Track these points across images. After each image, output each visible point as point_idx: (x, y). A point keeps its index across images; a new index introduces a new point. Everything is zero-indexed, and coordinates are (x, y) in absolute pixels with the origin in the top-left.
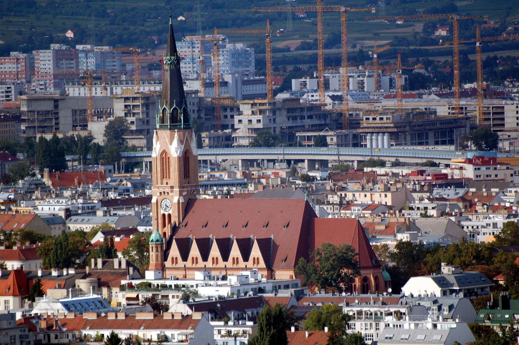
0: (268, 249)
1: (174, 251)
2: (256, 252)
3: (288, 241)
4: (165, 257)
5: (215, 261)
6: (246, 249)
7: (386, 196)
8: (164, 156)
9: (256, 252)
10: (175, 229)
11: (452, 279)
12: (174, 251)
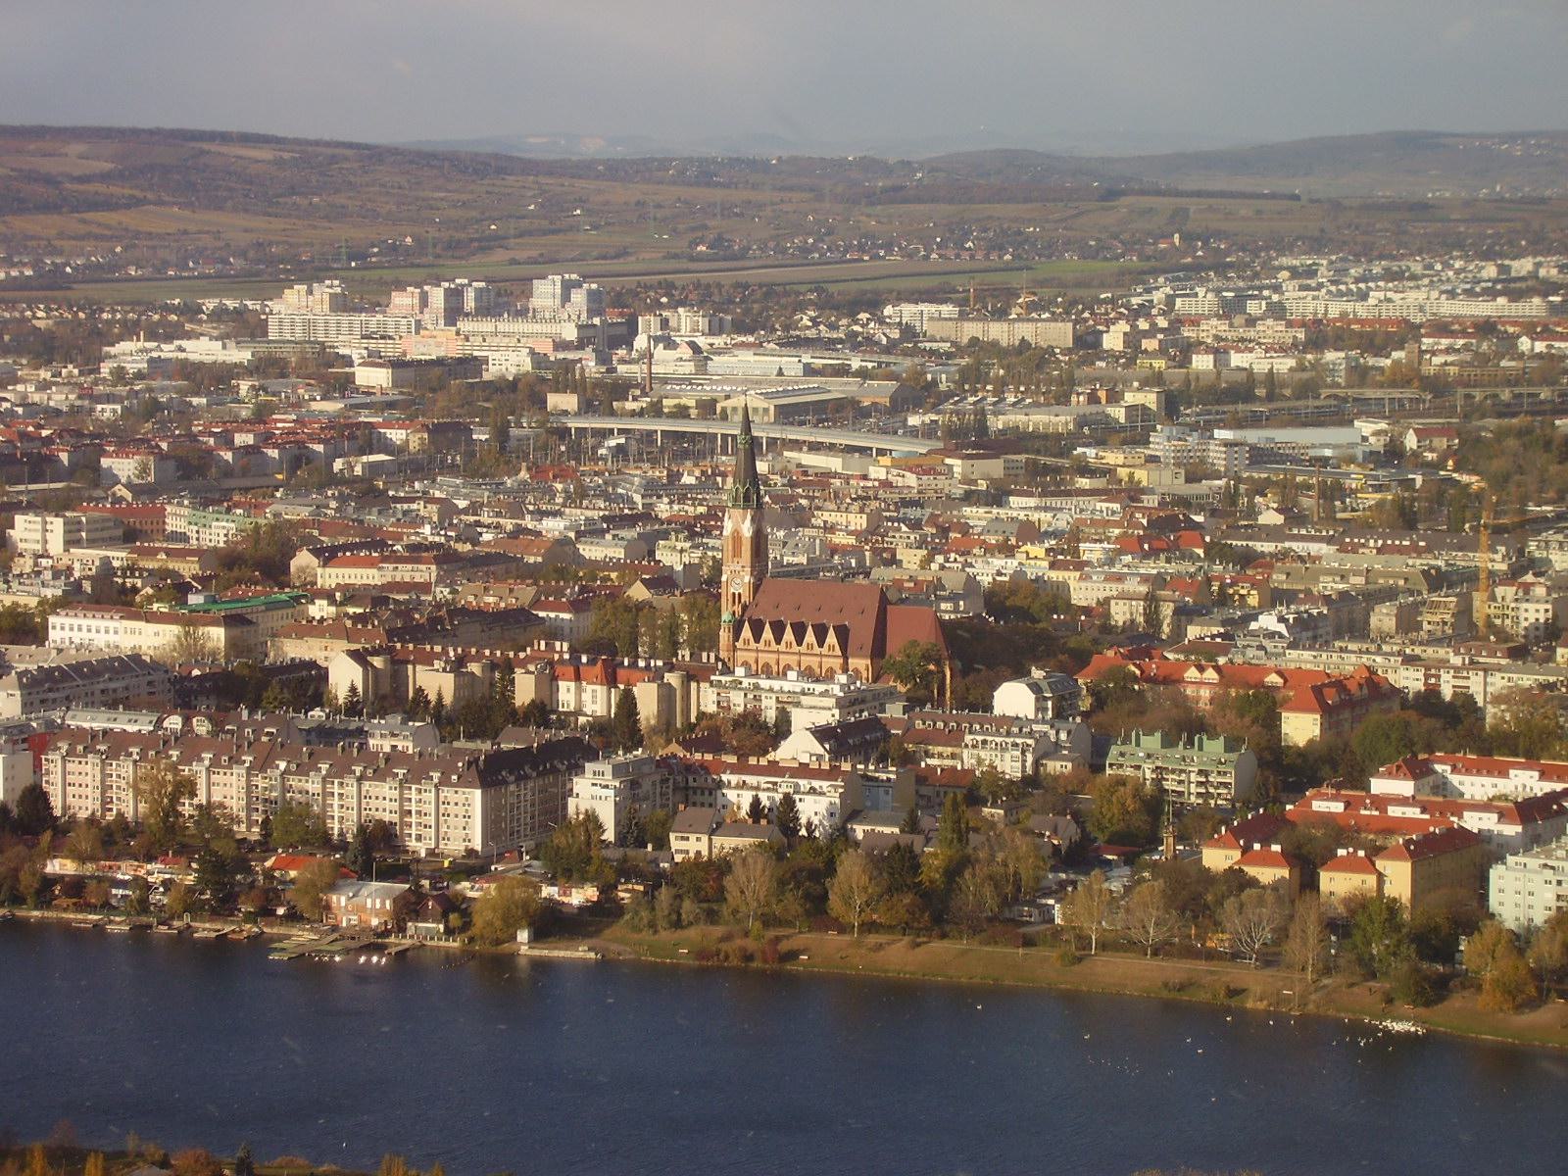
0: (843, 634)
1: (747, 632)
2: (831, 638)
3: (863, 631)
4: (737, 637)
5: (789, 645)
6: (821, 635)
7: (698, 839)
8: (737, 537)
9: (831, 638)
10: (745, 608)
11: (1044, 685)
12: (747, 632)
